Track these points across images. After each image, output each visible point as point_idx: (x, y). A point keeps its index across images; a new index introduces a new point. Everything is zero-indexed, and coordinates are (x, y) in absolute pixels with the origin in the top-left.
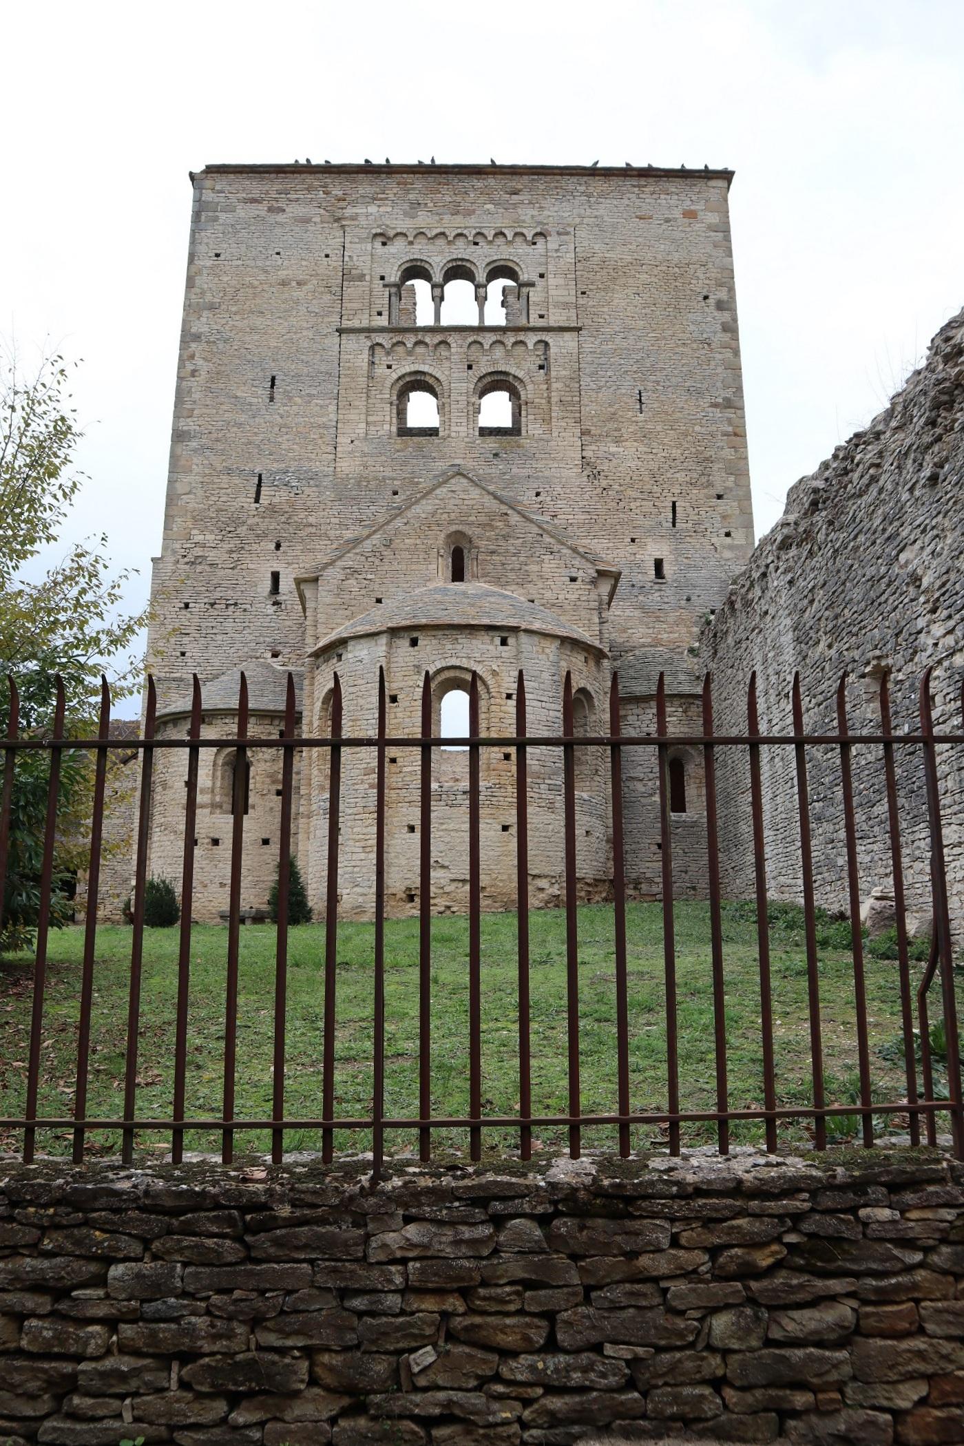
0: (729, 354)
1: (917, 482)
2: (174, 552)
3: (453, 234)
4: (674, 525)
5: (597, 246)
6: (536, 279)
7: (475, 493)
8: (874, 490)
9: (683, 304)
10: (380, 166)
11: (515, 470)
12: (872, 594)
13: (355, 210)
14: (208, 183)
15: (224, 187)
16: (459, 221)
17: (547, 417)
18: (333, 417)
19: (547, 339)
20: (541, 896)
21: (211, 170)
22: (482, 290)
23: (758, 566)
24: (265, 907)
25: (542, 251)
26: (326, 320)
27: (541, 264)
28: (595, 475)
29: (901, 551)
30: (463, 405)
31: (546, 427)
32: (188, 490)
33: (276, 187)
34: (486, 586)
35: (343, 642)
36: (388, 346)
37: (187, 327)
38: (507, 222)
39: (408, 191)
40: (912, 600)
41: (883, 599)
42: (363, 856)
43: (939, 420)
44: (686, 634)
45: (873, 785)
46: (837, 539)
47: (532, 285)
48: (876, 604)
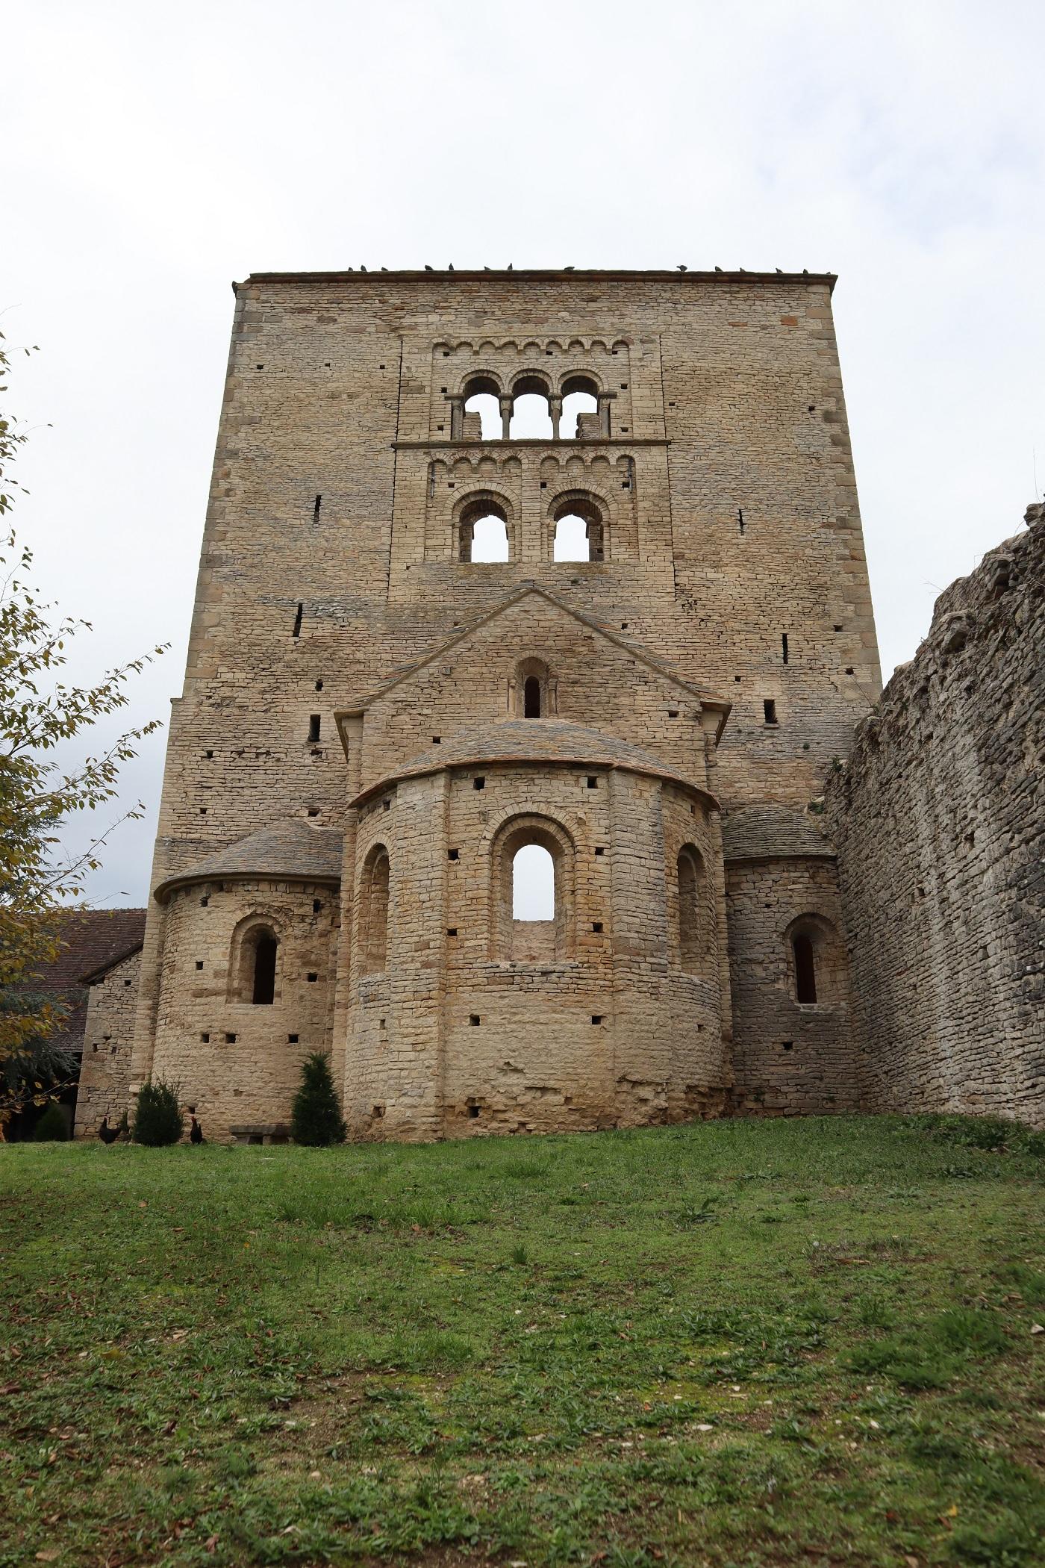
0: (841, 470)
2: (197, 692)
4: (786, 662)
5: (685, 356)
7: (552, 613)
10: (442, 273)
11: (597, 599)
14: (253, 293)
15: (268, 297)
16: (530, 329)
21: (257, 279)
22: (556, 403)
23: (912, 683)
25: (625, 361)
26: (380, 434)
27: (623, 374)
31: (632, 551)
32: (215, 621)
33: (328, 296)
35: (391, 786)
36: (449, 462)
37: (223, 443)
38: (583, 330)
39: (473, 300)
42: (412, 1055)
44: (805, 788)
47: (614, 396)
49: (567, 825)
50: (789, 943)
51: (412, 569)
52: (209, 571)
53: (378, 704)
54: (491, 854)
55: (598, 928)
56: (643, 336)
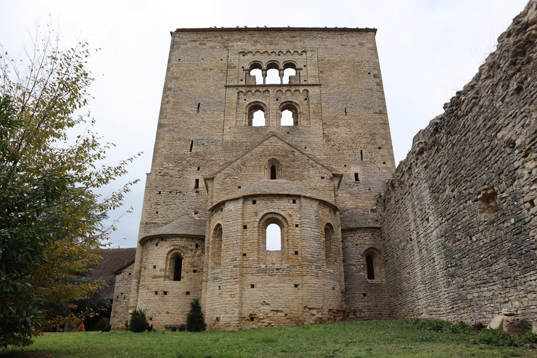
0: (380, 94)
1: (507, 94)
5: (326, 56)
6: (303, 67)
7: (280, 143)
8: (476, 109)
9: (361, 76)
10: (242, 28)
11: (296, 139)
14: (177, 35)
17: (308, 118)
19: (308, 89)
20: (313, 318)
21: (178, 30)
22: (281, 72)
24: (185, 323)
25: (305, 58)
26: (221, 82)
28: (329, 140)
29: (498, 132)
30: (274, 114)
32: (163, 146)
34: (285, 181)
35: (223, 203)
36: (245, 92)
39: (253, 37)
41: (488, 159)
42: (230, 299)
45: (490, 254)
46: (454, 138)
47: (301, 69)
49: (285, 217)
50: (364, 258)
53: (219, 175)
54: (258, 227)
55: (296, 253)
56: (311, 49)
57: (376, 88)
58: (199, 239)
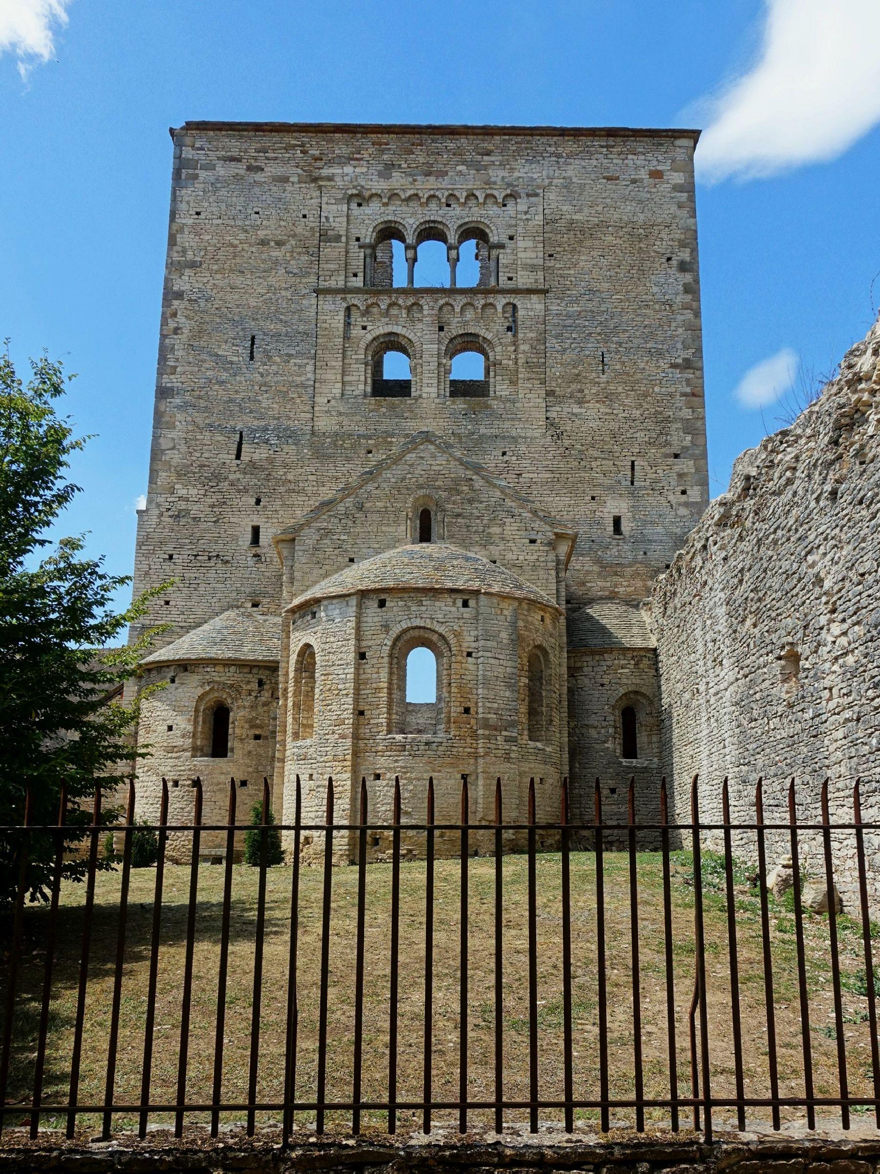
0: (689, 315)
1: (821, 494)
2: (159, 505)
3: (426, 196)
4: (632, 483)
5: (565, 208)
6: (506, 241)
11: (483, 431)
12: (787, 587)
13: (331, 171)
16: (432, 182)
18: (310, 376)
21: (190, 126)
22: (454, 253)
26: (304, 280)
27: (510, 226)
29: (809, 553)
31: (512, 389)
32: (171, 445)
39: (382, 152)
40: (817, 599)
41: (794, 592)
43: (841, 440)
47: (502, 246)
48: (789, 595)
50: (617, 713)
51: (333, 402)
52: (163, 402)
53: (306, 531)
55: (467, 711)
57: (682, 299)
58: (266, 668)
